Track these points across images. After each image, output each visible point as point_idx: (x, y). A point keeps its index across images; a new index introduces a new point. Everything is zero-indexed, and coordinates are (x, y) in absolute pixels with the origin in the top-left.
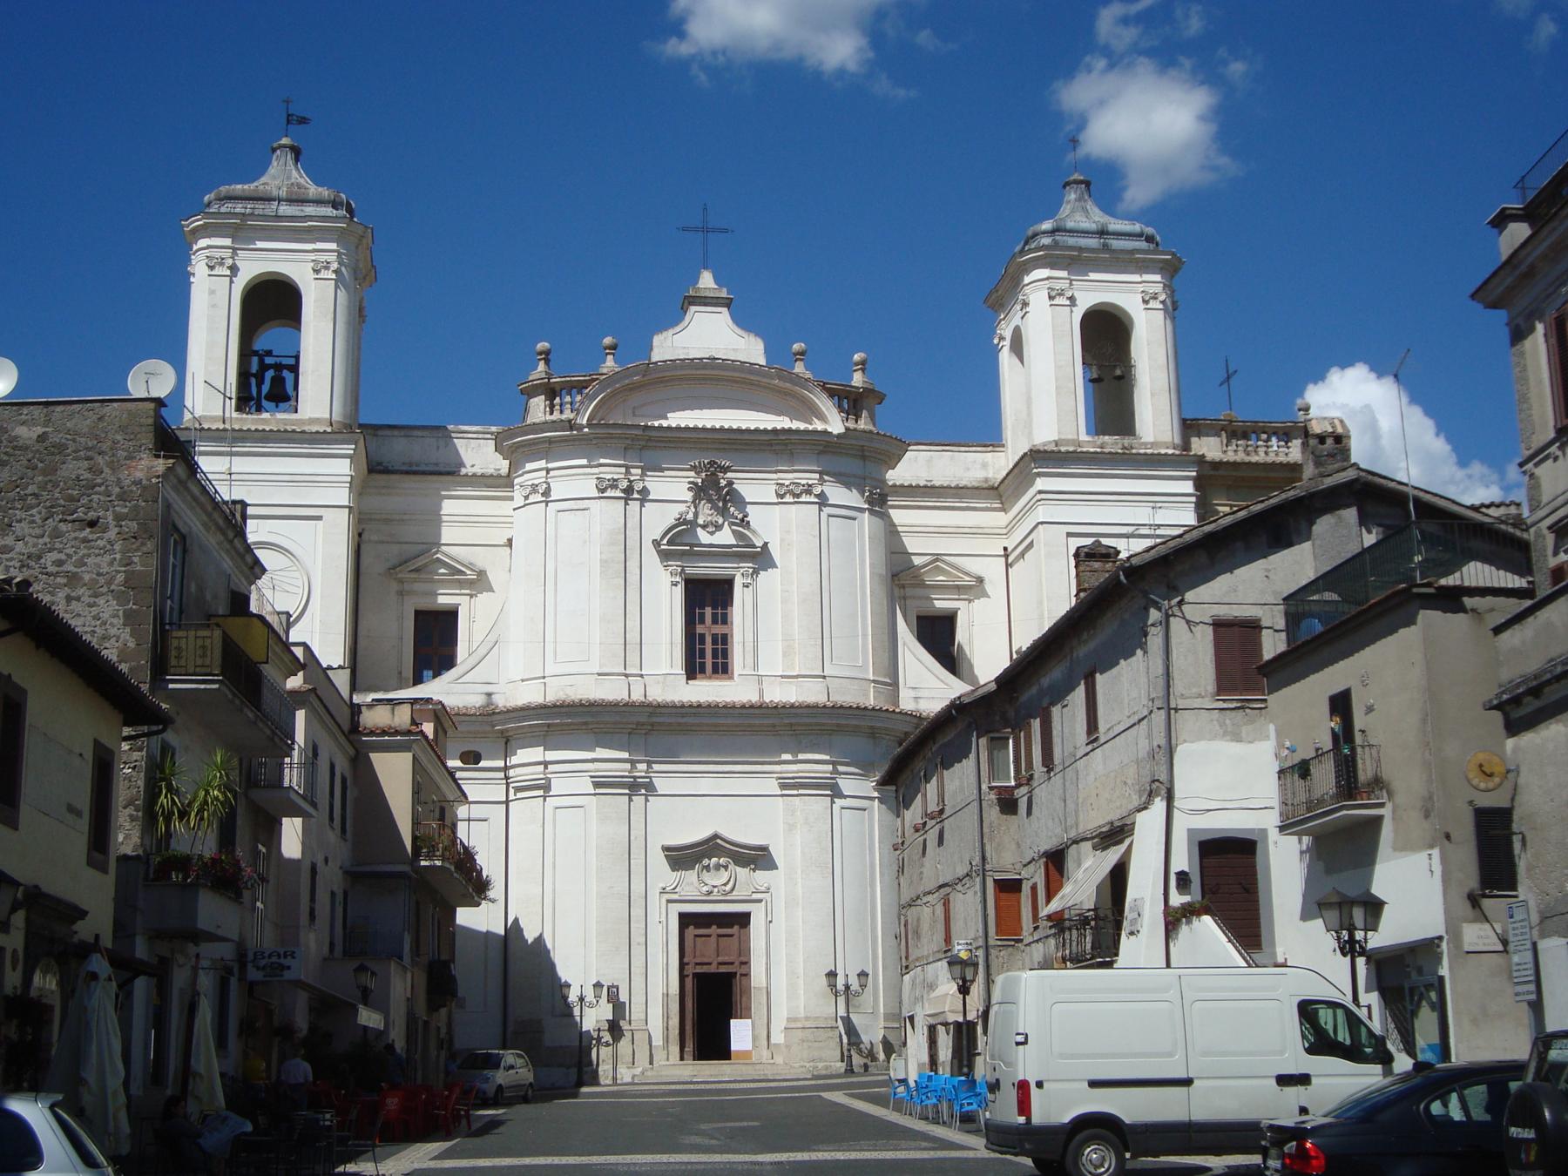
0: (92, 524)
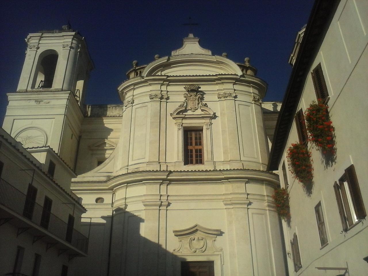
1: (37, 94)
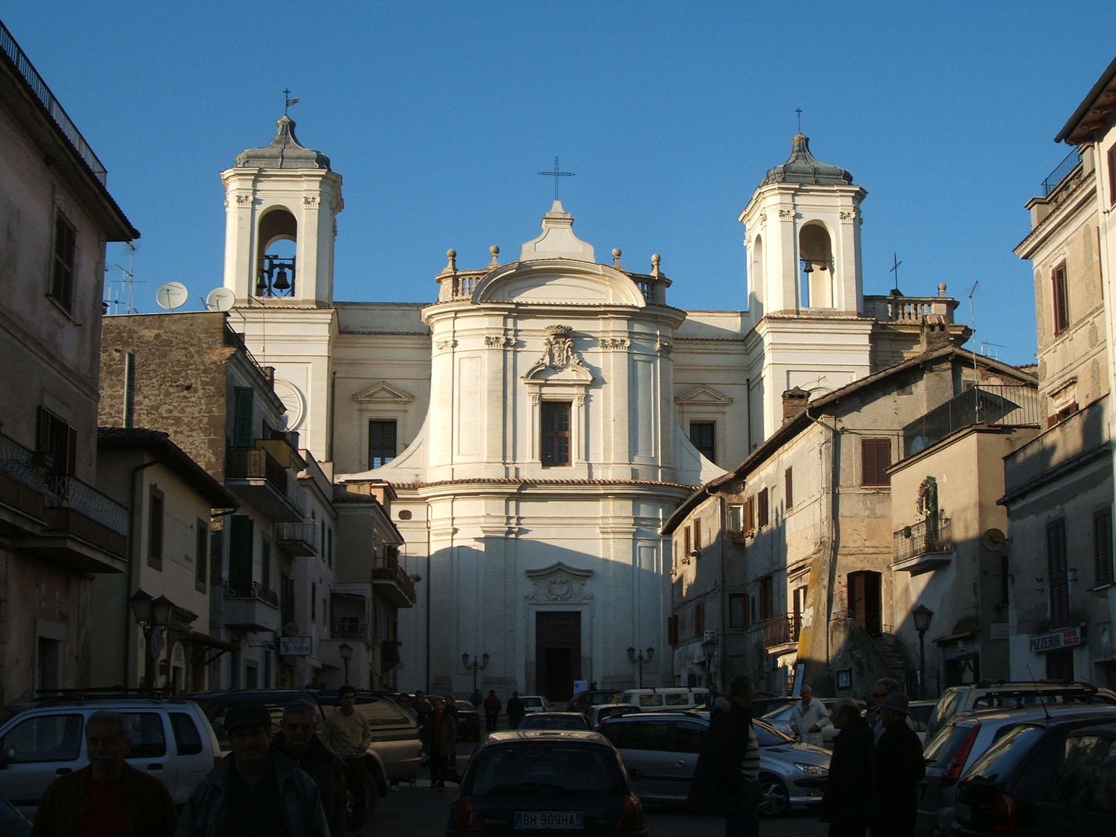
0: (188, 388)
1: (272, 313)
